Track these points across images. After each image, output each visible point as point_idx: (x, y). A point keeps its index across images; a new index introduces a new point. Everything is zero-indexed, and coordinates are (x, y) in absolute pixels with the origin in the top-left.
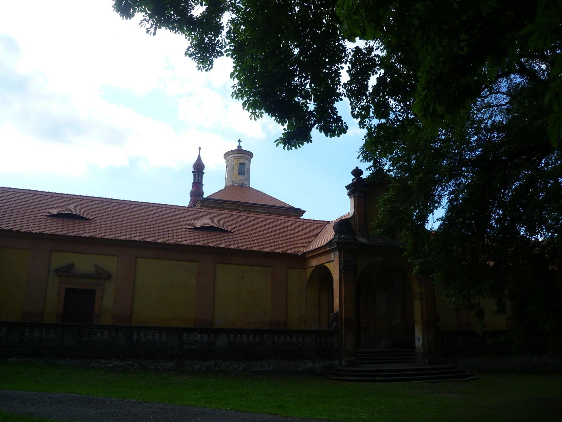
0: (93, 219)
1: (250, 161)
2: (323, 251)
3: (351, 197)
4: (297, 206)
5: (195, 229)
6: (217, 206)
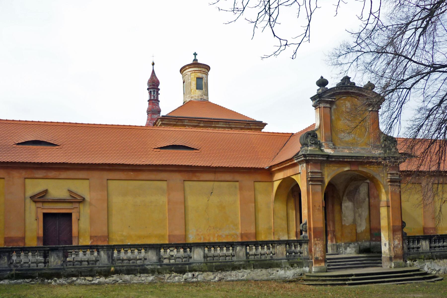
0: (61, 145)
1: (207, 74)
2: (290, 163)
3: (317, 109)
4: (258, 119)
5: (161, 148)
6: (178, 124)
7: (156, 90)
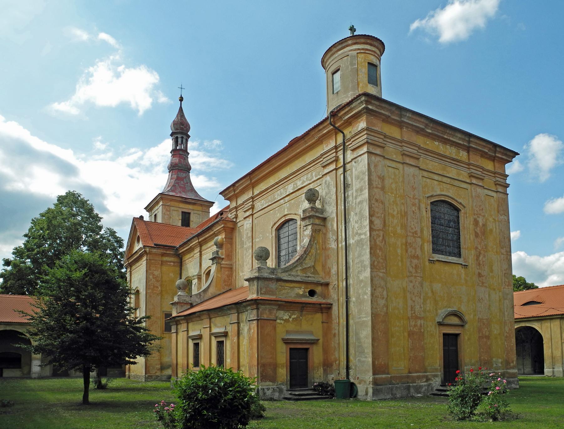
7: (185, 137)
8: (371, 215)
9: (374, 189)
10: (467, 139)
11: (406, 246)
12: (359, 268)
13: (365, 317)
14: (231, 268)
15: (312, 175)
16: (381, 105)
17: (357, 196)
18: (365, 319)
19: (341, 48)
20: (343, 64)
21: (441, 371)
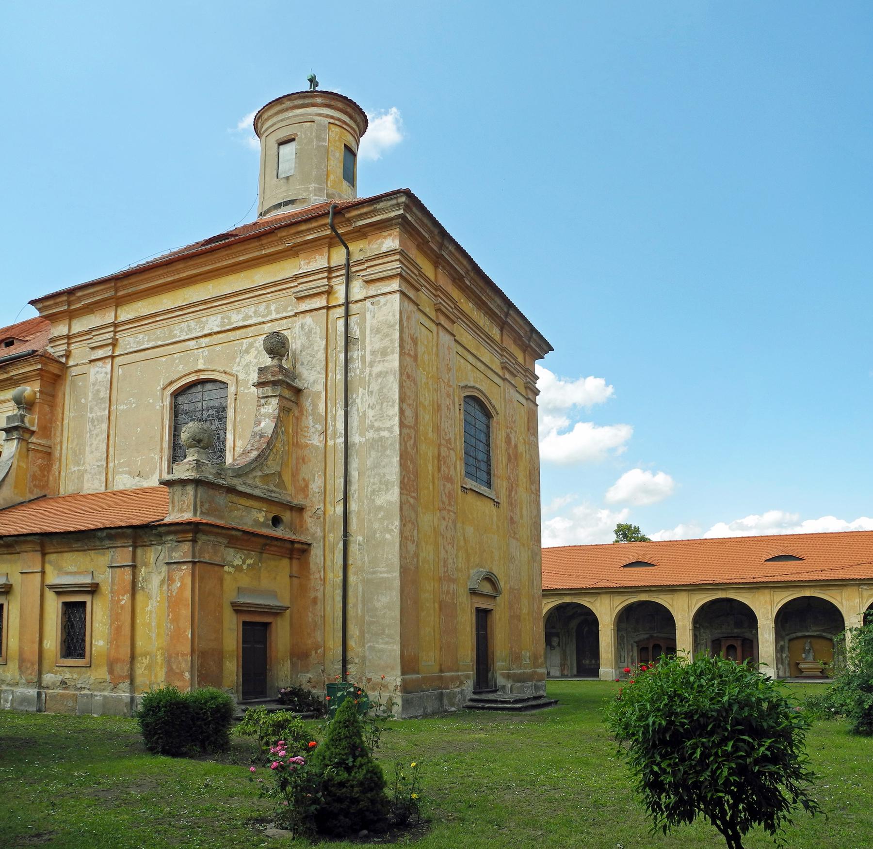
8: (402, 400)
9: (406, 356)
10: (506, 310)
11: (439, 461)
12: (374, 484)
13: (385, 572)
14: (48, 454)
15: (268, 307)
16: (423, 219)
17: (374, 362)
18: (385, 575)
19: (302, 104)
20: (302, 132)
21: (473, 670)
